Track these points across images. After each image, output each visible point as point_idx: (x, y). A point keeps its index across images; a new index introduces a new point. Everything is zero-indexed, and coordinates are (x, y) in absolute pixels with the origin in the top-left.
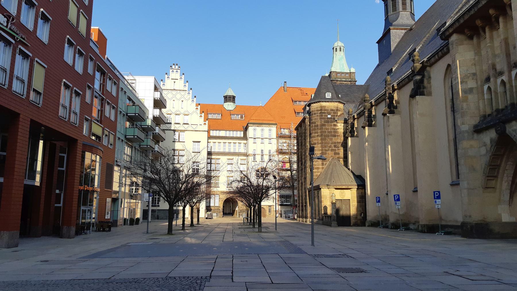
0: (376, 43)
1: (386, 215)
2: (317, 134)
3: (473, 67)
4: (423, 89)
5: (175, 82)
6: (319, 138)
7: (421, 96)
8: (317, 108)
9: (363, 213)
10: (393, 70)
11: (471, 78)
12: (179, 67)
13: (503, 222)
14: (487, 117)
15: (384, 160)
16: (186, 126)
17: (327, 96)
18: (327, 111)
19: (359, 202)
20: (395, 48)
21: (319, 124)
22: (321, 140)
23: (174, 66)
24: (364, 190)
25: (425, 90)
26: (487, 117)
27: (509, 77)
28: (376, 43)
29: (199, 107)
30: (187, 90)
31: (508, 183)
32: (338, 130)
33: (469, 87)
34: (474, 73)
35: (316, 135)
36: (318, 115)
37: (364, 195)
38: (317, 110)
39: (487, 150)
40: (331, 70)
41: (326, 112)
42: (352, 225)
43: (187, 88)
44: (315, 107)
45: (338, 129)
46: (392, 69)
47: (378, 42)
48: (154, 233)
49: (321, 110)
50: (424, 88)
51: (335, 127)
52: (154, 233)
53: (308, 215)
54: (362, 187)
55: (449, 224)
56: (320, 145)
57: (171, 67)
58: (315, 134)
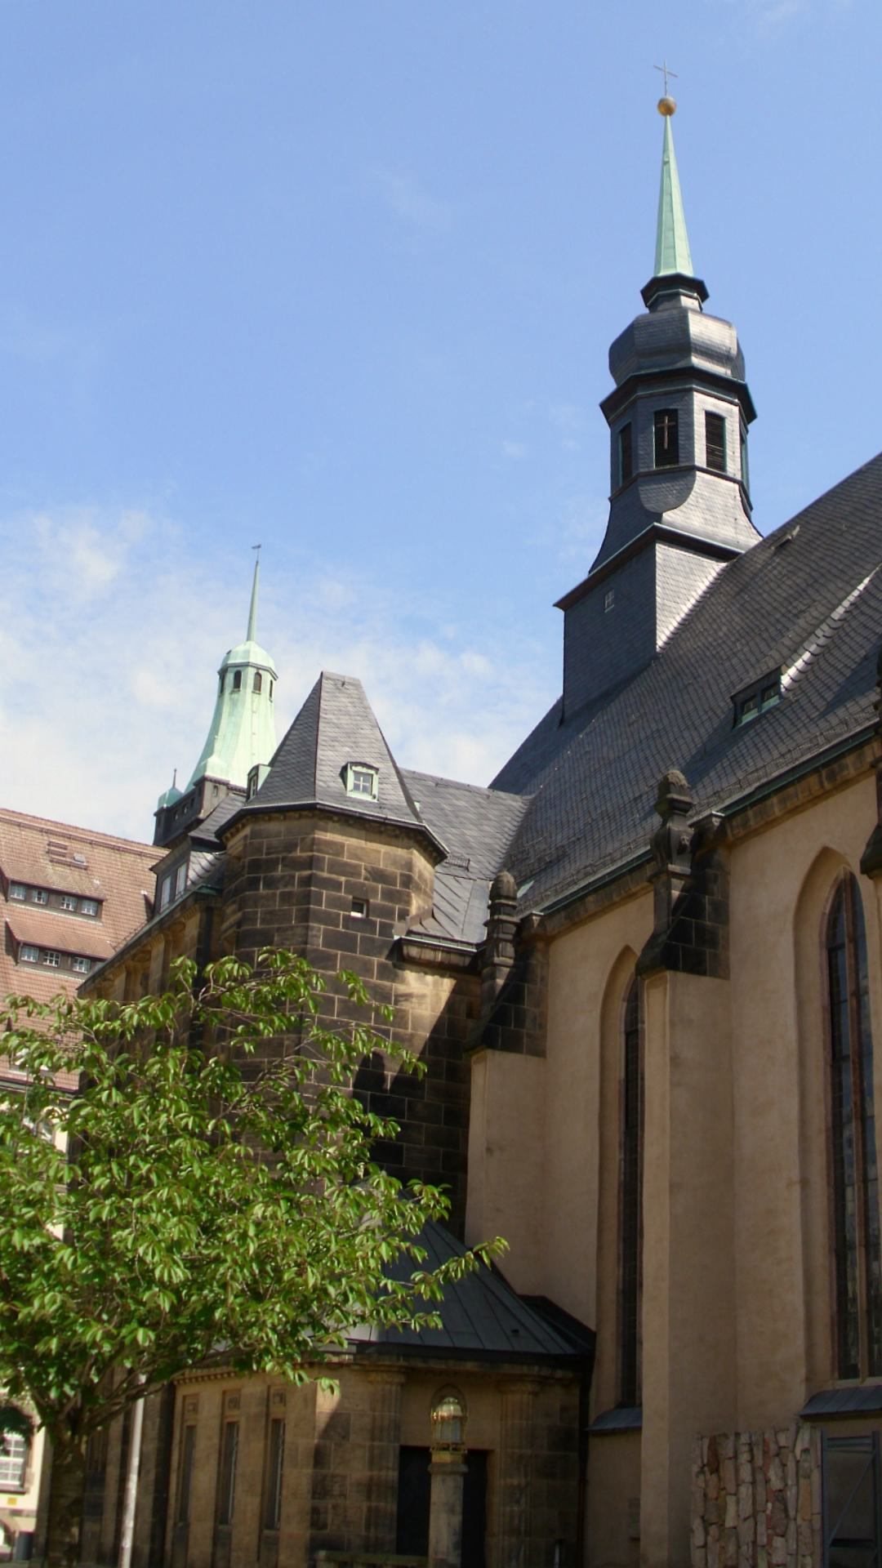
0: (558, 605)
2: (369, 982)
9: (561, 1542)
10: (785, 680)
18: (352, 875)
20: (686, 625)
24: (577, 1391)
28: (558, 605)
32: (404, 1006)
36: (290, 893)
37: (576, 1425)
40: (205, 770)
41: (343, 879)
45: (408, 997)
46: (777, 673)
47: (568, 603)
48: (460, 866)
51: (388, 979)
52: (460, 866)
54: (570, 1375)
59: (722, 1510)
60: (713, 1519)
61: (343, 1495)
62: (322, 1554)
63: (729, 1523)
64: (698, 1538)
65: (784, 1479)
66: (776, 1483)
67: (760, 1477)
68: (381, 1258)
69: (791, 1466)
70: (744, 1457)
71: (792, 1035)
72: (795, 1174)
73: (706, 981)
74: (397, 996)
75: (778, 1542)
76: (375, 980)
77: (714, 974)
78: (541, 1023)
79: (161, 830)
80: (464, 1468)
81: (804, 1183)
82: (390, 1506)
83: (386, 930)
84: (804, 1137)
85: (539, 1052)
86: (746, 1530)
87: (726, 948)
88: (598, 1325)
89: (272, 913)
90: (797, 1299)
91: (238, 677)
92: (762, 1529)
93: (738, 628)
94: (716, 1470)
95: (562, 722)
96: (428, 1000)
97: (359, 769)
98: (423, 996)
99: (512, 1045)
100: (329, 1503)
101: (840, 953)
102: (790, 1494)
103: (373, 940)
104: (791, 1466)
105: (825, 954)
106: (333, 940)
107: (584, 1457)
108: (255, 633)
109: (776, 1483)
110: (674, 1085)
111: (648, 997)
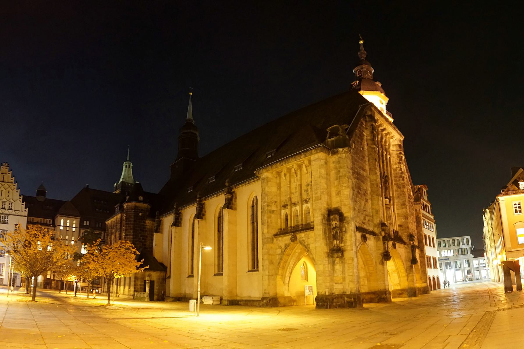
1: (185, 293)
4: (232, 205)
5: (4, 176)
6: (132, 231)
7: (230, 210)
8: (131, 207)
11: (273, 204)
12: (8, 165)
16: (10, 211)
17: (140, 199)
19: (53, 296)
21: (132, 220)
22: (133, 232)
23: (4, 164)
25: (233, 206)
29: (22, 197)
30: (13, 182)
33: (272, 209)
35: (129, 228)
39: (281, 251)
42: (154, 300)
43: (13, 181)
45: (146, 225)
49: (135, 209)
50: (233, 204)
53: (47, 301)
55: (244, 299)
56: (131, 237)
57: (2, 164)
58: (128, 227)
61: (138, 286)
62: (135, 292)
68: (372, 80)
73: (179, 227)
76: (142, 223)
77: (180, 227)
78: (162, 230)
81: (189, 252)
85: (162, 233)
87: (182, 224)
93: (127, 287)
99: (158, 232)
100: (136, 286)
101: (281, 173)
105: (192, 226)
107: (166, 281)
110: (175, 240)
111: (112, 286)
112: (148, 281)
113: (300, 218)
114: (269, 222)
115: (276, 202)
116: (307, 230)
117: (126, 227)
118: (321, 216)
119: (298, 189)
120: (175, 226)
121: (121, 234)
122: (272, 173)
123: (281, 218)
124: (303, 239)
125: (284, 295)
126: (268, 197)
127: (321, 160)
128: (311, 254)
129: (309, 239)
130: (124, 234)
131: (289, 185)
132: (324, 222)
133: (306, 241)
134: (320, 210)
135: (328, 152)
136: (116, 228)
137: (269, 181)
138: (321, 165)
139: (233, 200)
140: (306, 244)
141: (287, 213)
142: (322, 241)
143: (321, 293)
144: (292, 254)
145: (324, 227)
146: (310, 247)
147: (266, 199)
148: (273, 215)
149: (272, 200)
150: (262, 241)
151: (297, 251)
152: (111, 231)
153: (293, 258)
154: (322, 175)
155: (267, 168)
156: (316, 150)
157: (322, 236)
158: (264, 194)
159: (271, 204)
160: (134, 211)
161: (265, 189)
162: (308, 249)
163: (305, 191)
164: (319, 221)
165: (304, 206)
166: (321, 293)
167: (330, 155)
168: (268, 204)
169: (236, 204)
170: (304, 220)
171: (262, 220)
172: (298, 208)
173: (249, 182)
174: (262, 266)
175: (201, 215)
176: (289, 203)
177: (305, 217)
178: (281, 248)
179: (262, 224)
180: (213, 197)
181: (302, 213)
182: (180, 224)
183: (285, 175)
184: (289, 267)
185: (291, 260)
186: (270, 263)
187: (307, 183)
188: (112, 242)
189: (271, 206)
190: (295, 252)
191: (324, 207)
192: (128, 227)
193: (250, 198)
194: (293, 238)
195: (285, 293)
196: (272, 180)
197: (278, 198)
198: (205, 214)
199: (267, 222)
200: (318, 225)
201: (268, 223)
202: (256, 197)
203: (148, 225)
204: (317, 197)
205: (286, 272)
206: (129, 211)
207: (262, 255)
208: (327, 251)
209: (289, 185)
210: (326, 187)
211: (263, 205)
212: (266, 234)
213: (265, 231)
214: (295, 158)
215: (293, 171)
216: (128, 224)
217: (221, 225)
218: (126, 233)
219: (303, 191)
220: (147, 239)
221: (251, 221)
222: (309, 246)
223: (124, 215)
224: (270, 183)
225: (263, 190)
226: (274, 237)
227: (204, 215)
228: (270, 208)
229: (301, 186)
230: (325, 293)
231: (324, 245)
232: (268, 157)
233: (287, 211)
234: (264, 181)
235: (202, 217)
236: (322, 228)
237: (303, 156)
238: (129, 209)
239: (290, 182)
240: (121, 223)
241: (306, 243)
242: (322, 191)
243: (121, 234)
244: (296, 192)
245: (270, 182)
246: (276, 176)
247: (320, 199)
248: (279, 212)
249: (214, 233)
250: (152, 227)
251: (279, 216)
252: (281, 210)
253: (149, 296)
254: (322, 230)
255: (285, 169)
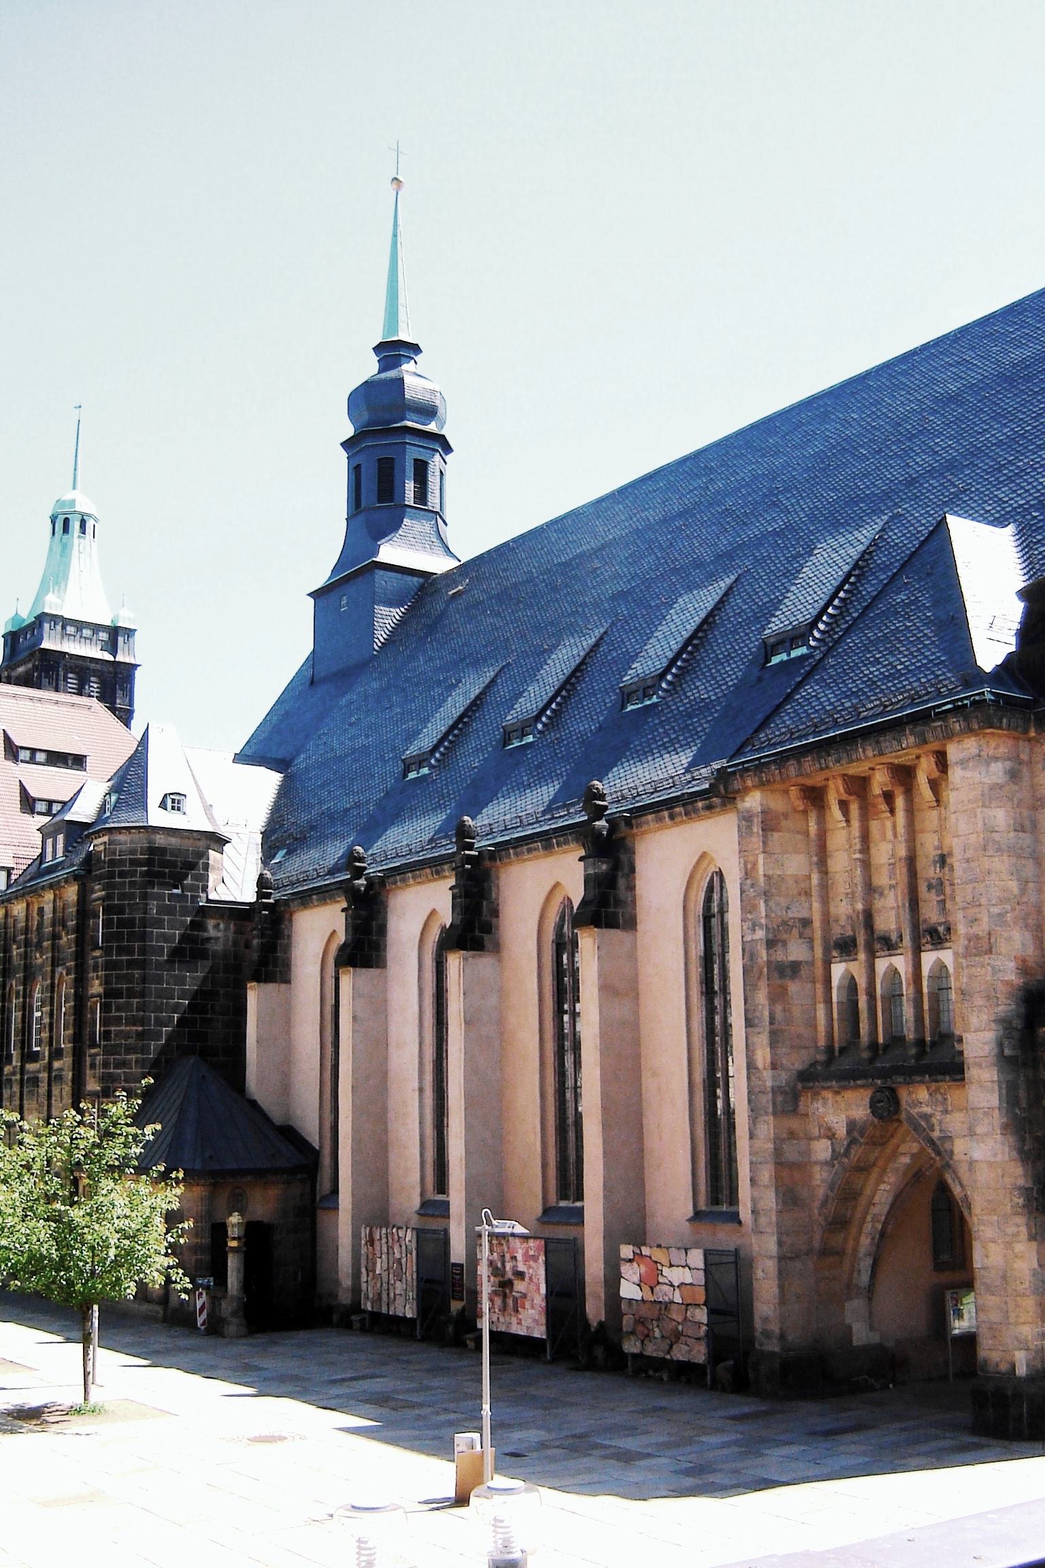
3: (803, 898)
4: (616, 907)
8: (133, 852)
11: (795, 931)
13: (857, 1346)
14: (837, 1054)
15: (417, 1093)
26: (837, 1054)
27: (914, 966)
31: (873, 1239)
32: (208, 946)
33: (792, 958)
34: (804, 919)
38: (134, 862)
39: (833, 1151)
44: (124, 847)
45: (209, 939)
49: (149, 862)
50: (618, 902)
59: (374, 1264)
60: (371, 1270)
63: (378, 1272)
64: (364, 1278)
65: (401, 1253)
66: (397, 1255)
67: (391, 1251)
69: (404, 1247)
70: (384, 1240)
71: (416, 1008)
72: (416, 1085)
74: (202, 940)
75: (398, 1284)
77: (378, 967)
79: (8, 651)
80: (245, 1249)
81: (421, 1090)
82: (206, 1258)
83: (195, 899)
84: (421, 1064)
86: (385, 1275)
88: (320, 1147)
89: (124, 894)
90: (415, 1150)
91: (66, 521)
92: (391, 1276)
94: (372, 1245)
95: (312, 683)
96: (221, 940)
97: (172, 796)
98: (218, 938)
102: (404, 1261)
103: (186, 907)
104: (404, 1247)
106: (163, 910)
108: (79, 484)
109: (397, 1255)
112: (234, 1239)
113: (908, 1012)
114: (779, 1015)
115: (806, 922)
116: (939, 1077)
117: (107, 951)
118: (993, 1026)
119: (902, 874)
120: (354, 966)
121: (80, 982)
122: (786, 792)
123: (828, 1001)
124: (927, 1110)
125: (851, 1341)
126: (771, 904)
127: (988, 765)
128: (958, 1178)
129: (946, 1112)
130: (96, 988)
131: (858, 856)
132: (1007, 1052)
133: (934, 1120)
134: (988, 998)
135: (1020, 722)
136: (55, 948)
137: (773, 830)
138: (993, 787)
139: (622, 883)
140: (936, 1134)
141: (853, 978)
142: (999, 1137)
143: (997, 1364)
144: (881, 1163)
145: (1010, 1077)
146: (952, 1152)
147: (763, 914)
148: (793, 987)
149: (790, 915)
150: (749, 1101)
151: (902, 1149)
152: (25, 956)
153: (886, 1179)
154: (996, 836)
155: (761, 772)
156: (966, 719)
157: (997, 1119)
158: (752, 885)
159: (785, 936)
160: (143, 874)
161: (755, 864)
162: (947, 1158)
163: (930, 887)
164: (987, 1048)
165: (929, 959)
166: (997, 1364)
167: (1032, 734)
168: (771, 936)
169: (634, 902)
170: (927, 1022)
171: (745, 1004)
172: (901, 963)
173: (689, 807)
174: (753, 1212)
175: (477, 933)
176: (861, 940)
177: (930, 1009)
178: (831, 1136)
179: (749, 1023)
180: (529, 851)
181: (919, 991)
182: (374, 954)
183: (844, 805)
184: (869, 1218)
185: (878, 1185)
186: (784, 1203)
187: (939, 852)
188: (31, 1013)
189: (785, 943)
190: (894, 1155)
191: (1007, 983)
192: (121, 951)
193: (698, 876)
194: (880, 1101)
195: (854, 1330)
196: (784, 823)
197: (816, 905)
198: (494, 920)
199: (767, 1019)
200: (980, 1066)
201: (771, 1023)
202: (720, 874)
203: (217, 939)
204: (977, 937)
205: (857, 1240)
206: (122, 874)
207: (751, 1163)
208: (1021, 1182)
209: (861, 852)
210: (1016, 891)
211: (748, 938)
212: (765, 1073)
213: (763, 1056)
214: (878, 742)
215: (876, 790)
216: (118, 937)
217: (571, 1135)
218: (106, 981)
219: (922, 888)
220: (212, 1006)
221: (701, 983)
222: (947, 1146)
223: (93, 892)
224: (776, 835)
225: (749, 866)
226: (800, 1086)
227: (489, 928)
228: (780, 956)
229: (911, 861)
230: (1014, 1367)
231: (1007, 1157)
232: (775, 660)
233: (857, 968)
234: (749, 827)
235: (482, 938)
236: (999, 1082)
237: (912, 739)
238: (122, 862)
239: (865, 837)
240: (81, 930)
241: (937, 1128)
242: (995, 910)
243: (80, 982)
244: (891, 887)
245: (779, 831)
246: (802, 808)
247: (990, 951)
248: (819, 971)
249: (537, 1077)
250: (235, 944)
251: (820, 988)
252: (827, 964)
253: (241, 1313)
254: (1000, 1087)
255: (840, 782)
